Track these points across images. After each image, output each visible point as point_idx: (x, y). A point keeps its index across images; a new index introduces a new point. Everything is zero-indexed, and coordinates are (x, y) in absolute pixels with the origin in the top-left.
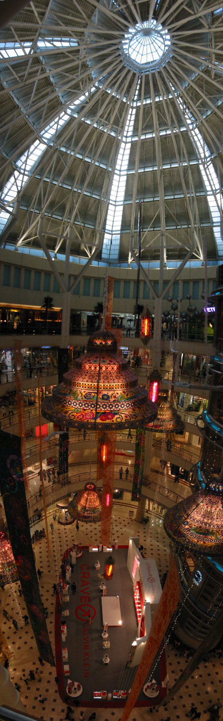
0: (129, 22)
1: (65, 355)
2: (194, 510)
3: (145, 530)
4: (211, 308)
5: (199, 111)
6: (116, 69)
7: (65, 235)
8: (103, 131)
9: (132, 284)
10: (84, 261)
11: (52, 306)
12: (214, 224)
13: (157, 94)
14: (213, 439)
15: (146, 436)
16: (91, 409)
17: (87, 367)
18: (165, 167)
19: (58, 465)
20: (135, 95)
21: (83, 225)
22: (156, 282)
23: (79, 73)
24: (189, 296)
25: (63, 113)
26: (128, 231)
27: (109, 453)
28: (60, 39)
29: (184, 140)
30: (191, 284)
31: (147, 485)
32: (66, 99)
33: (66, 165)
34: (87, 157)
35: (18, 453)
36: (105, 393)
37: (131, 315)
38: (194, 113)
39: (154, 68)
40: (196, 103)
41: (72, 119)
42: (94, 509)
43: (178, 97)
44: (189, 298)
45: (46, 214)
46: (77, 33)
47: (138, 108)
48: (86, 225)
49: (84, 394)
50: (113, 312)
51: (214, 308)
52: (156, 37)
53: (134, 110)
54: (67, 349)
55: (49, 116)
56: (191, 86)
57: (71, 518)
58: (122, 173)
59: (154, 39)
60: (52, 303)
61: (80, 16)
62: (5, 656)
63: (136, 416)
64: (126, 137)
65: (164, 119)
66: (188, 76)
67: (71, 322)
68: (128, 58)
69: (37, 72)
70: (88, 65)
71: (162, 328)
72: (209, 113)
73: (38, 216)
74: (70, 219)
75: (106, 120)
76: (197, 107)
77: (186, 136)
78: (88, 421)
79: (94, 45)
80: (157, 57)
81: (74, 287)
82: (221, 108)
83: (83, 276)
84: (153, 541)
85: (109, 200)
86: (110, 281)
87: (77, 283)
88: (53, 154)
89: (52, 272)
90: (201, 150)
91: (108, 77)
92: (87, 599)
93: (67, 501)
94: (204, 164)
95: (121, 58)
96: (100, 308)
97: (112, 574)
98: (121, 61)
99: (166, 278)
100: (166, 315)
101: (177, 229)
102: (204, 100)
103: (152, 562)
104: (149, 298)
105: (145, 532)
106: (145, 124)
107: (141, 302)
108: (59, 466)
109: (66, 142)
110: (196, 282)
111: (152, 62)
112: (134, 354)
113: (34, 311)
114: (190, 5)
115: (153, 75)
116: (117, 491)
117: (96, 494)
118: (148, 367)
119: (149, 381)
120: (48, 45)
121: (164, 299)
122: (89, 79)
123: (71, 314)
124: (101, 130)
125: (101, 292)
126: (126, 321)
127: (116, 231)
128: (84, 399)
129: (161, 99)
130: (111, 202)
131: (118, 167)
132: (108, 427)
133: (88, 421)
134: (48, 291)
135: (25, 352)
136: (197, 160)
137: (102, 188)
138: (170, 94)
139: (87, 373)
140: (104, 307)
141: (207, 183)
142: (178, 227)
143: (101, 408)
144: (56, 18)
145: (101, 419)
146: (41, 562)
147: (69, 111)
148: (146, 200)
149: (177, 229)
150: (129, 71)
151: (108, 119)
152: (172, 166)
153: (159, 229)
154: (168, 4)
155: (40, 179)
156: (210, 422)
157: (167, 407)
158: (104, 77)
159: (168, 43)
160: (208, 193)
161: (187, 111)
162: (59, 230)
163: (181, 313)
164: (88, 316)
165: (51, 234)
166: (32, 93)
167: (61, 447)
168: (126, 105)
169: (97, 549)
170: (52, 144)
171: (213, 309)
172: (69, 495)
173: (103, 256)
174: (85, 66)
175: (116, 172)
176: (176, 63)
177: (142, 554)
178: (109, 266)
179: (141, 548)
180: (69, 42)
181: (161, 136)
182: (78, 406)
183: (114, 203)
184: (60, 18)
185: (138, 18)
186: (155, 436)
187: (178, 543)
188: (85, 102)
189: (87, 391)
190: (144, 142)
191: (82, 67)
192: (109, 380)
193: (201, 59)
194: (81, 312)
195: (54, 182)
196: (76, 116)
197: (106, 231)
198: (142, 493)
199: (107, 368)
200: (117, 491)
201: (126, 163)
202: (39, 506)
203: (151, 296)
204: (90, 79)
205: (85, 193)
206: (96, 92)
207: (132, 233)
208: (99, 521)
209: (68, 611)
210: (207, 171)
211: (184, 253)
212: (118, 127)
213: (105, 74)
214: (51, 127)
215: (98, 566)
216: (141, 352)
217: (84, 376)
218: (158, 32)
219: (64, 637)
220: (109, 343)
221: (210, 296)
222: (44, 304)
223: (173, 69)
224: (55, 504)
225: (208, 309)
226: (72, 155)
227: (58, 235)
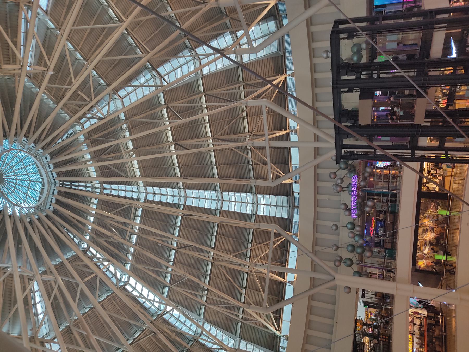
47: (102, 183)
98: (47, 216)
111: (43, 185)
142: (245, 114)
147: (125, 278)
173: (285, 216)
176: (33, 134)
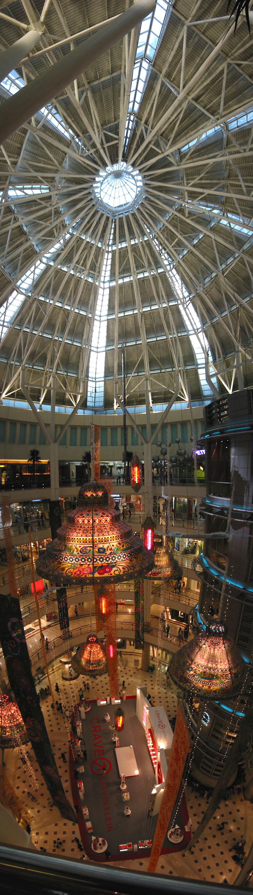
0: (99, 166)
1: (57, 508)
2: (197, 653)
3: (151, 679)
4: (201, 451)
5: (176, 250)
6: (89, 214)
7: (48, 385)
8: (80, 278)
9: (119, 431)
10: (69, 410)
11: (39, 458)
12: (199, 366)
13: (132, 237)
14: (211, 583)
15: (144, 584)
16: (88, 563)
17: (80, 521)
18: (144, 310)
19: (58, 620)
20: (109, 240)
21: (66, 374)
22: (144, 427)
23: (53, 220)
24: (178, 439)
25: (39, 262)
26: (111, 378)
27: (108, 605)
28: (30, 186)
29: (162, 281)
30: (179, 427)
31: (149, 632)
32: (41, 248)
33: (46, 314)
34: (67, 305)
35: (19, 614)
36: (101, 546)
37: (121, 462)
38: (170, 254)
39: (127, 211)
40: (172, 243)
41: (48, 267)
42: (99, 662)
43: (153, 239)
44: (178, 442)
45: (26, 366)
46: (48, 180)
47: (113, 252)
48: (69, 374)
49: (80, 549)
50: (101, 460)
51: (204, 451)
52: (127, 179)
53: (110, 255)
54: (59, 501)
55: (25, 265)
56: (166, 227)
57: (76, 673)
58: (102, 319)
59: (126, 181)
60: (39, 456)
61: (52, 163)
62: (26, 821)
63: (133, 567)
64: (104, 282)
65: (141, 261)
66: (163, 216)
67: (60, 474)
68: (100, 202)
69: (9, 221)
70: (61, 212)
71: (153, 473)
72: (185, 252)
73: (19, 368)
74: (52, 369)
75: (82, 265)
76: (173, 247)
77: (164, 277)
78: (86, 576)
79: (66, 190)
80: (130, 199)
81: (60, 439)
82: (197, 247)
83: (70, 426)
84: (161, 689)
85: (91, 346)
86: (96, 430)
87: (63, 434)
88: (32, 304)
89: (38, 423)
90: (179, 292)
91: (82, 223)
92: (101, 752)
93: (70, 656)
94: (183, 304)
95: (94, 202)
96: (88, 457)
97: (123, 725)
98: (93, 205)
99: (153, 422)
100: (156, 461)
101: (161, 372)
102: (180, 240)
103: (161, 709)
104: (137, 444)
105: (151, 681)
106: (122, 268)
107: (130, 449)
108: (60, 621)
109: (44, 292)
110: (184, 424)
111: (125, 205)
112: (126, 501)
113: (21, 465)
114: (157, 144)
115: (127, 217)
116: (119, 640)
117: (99, 646)
118: (141, 513)
119: (143, 529)
120: (19, 193)
121: (153, 444)
122: (63, 225)
123: (59, 465)
124: (78, 277)
125: (88, 443)
126: (116, 469)
127: (99, 378)
128: (80, 554)
129: (137, 242)
130: (92, 348)
131: (97, 313)
132: (107, 581)
133: (86, 576)
134: (34, 443)
135: (16, 507)
136: (176, 300)
137: (83, 335)
138: (145, 236)
139: (81, 527)
140: (92, 458)
141: (187, 323)
142: (163, 371)
143: (98, 561)
144: (27, 166)
145: (99, 573)
146: (50, 720)
147: (44, 260)
148: (128, 345)
149: (161, 372)
150: (102, 215)
151: (84, 265)
152: (152, 308)
153: (143, 373)
154: (137, 145)
155: (20, 330)
156: (208, 566)
157: (164, 553)
158: (77, 223)
159: (140, 184)
160: (190, 333)
161: (163, 251)
162: (41, 380)
163: (171, 458)
164: (76, 466)
165: (34, 385)
166: (6, 244)
167: (59, 602)
168: (102, 250)
169: (105, 702)
170: (30, 294)
171: (203, 452)
172: (72, 650)
173: (89, 404)
174: (57, 213)
175: (96, 317)
177: (150, 702)
178: (95, 414)
179: (149, 697)
180: (40, 189)
181: (139, 279)
182: (74, 561)
183: (95, 350)
184: (31, 166)
185: (107, 161)
186: (153, 583)
187: (184, 690)
188: (60, 249)
189: (82, 546)
190: (121, 287)
191: (55, 214)
192: (104, 532)
193: (174, 198)
194: (69, 463)
195: (34, 332)
196: (52, 263)
197: (89, 379)
198: (145, 641)
199: (101, 521)
200: (119, 640)
201: (105, 308)
202: (42, 664)
203: (139, 442)
204: (64, 226)
205: (66, 341)
206: (70, 239)
207: (116, 379)
208: (105, 673)
209: (83, 767)
210: (187, 310)
211: (169, 395)
212: (95, 272)
213: (78, 220)
214: (28, 277)
215: (108, 718)
216: (133, 499)
217: (78, 531)
218: (129, 174)
219: (81, 794)
220: (100, 494)
221: (199, 439)
222: (31, 457)
223: (146, 210)
224: (58, 660)
225: (198, 452)
226: (51, 304)
227: (41, 386)
